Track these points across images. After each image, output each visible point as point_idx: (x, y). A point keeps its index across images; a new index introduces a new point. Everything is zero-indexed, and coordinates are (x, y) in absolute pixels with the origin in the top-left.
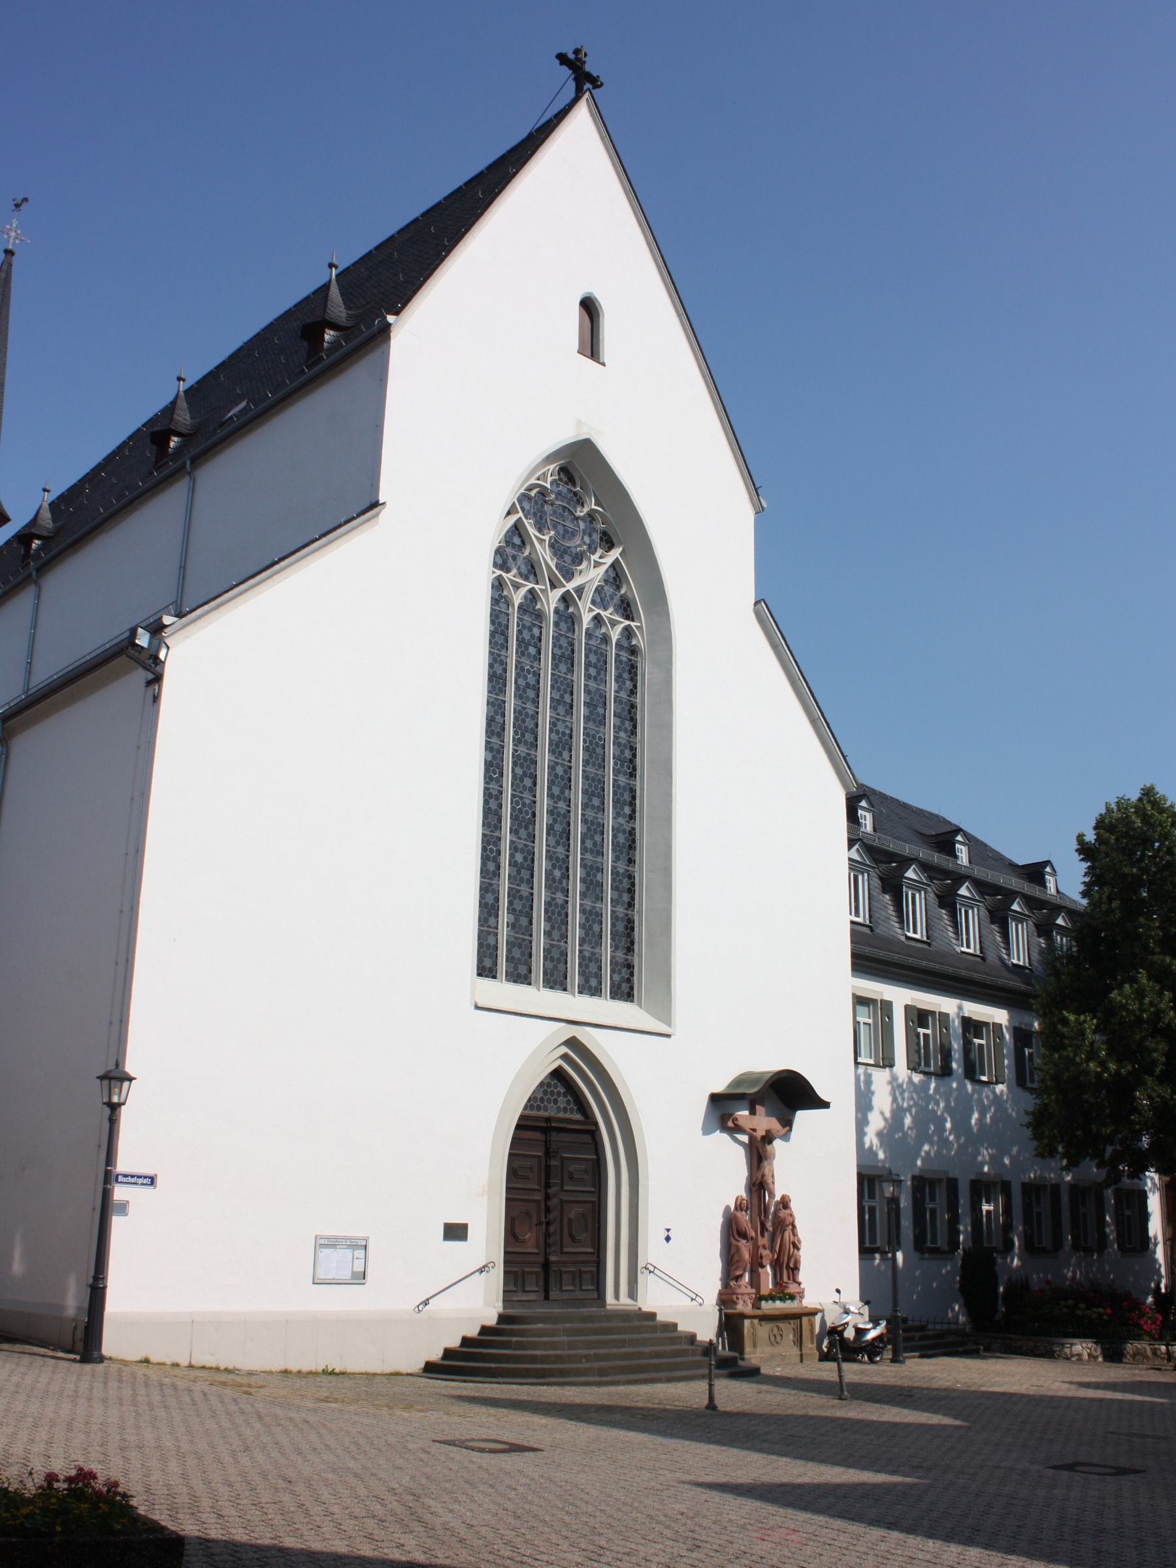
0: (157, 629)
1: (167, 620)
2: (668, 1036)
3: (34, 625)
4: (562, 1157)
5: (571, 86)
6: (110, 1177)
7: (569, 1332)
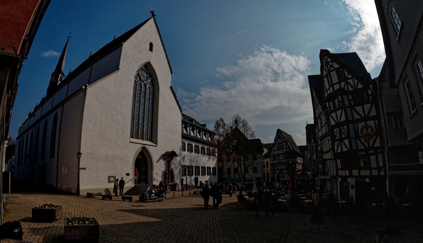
0: (86, 86)
1: (87, 85)
4: (143, 162)
5: (151, 16)
6: (79, 169)
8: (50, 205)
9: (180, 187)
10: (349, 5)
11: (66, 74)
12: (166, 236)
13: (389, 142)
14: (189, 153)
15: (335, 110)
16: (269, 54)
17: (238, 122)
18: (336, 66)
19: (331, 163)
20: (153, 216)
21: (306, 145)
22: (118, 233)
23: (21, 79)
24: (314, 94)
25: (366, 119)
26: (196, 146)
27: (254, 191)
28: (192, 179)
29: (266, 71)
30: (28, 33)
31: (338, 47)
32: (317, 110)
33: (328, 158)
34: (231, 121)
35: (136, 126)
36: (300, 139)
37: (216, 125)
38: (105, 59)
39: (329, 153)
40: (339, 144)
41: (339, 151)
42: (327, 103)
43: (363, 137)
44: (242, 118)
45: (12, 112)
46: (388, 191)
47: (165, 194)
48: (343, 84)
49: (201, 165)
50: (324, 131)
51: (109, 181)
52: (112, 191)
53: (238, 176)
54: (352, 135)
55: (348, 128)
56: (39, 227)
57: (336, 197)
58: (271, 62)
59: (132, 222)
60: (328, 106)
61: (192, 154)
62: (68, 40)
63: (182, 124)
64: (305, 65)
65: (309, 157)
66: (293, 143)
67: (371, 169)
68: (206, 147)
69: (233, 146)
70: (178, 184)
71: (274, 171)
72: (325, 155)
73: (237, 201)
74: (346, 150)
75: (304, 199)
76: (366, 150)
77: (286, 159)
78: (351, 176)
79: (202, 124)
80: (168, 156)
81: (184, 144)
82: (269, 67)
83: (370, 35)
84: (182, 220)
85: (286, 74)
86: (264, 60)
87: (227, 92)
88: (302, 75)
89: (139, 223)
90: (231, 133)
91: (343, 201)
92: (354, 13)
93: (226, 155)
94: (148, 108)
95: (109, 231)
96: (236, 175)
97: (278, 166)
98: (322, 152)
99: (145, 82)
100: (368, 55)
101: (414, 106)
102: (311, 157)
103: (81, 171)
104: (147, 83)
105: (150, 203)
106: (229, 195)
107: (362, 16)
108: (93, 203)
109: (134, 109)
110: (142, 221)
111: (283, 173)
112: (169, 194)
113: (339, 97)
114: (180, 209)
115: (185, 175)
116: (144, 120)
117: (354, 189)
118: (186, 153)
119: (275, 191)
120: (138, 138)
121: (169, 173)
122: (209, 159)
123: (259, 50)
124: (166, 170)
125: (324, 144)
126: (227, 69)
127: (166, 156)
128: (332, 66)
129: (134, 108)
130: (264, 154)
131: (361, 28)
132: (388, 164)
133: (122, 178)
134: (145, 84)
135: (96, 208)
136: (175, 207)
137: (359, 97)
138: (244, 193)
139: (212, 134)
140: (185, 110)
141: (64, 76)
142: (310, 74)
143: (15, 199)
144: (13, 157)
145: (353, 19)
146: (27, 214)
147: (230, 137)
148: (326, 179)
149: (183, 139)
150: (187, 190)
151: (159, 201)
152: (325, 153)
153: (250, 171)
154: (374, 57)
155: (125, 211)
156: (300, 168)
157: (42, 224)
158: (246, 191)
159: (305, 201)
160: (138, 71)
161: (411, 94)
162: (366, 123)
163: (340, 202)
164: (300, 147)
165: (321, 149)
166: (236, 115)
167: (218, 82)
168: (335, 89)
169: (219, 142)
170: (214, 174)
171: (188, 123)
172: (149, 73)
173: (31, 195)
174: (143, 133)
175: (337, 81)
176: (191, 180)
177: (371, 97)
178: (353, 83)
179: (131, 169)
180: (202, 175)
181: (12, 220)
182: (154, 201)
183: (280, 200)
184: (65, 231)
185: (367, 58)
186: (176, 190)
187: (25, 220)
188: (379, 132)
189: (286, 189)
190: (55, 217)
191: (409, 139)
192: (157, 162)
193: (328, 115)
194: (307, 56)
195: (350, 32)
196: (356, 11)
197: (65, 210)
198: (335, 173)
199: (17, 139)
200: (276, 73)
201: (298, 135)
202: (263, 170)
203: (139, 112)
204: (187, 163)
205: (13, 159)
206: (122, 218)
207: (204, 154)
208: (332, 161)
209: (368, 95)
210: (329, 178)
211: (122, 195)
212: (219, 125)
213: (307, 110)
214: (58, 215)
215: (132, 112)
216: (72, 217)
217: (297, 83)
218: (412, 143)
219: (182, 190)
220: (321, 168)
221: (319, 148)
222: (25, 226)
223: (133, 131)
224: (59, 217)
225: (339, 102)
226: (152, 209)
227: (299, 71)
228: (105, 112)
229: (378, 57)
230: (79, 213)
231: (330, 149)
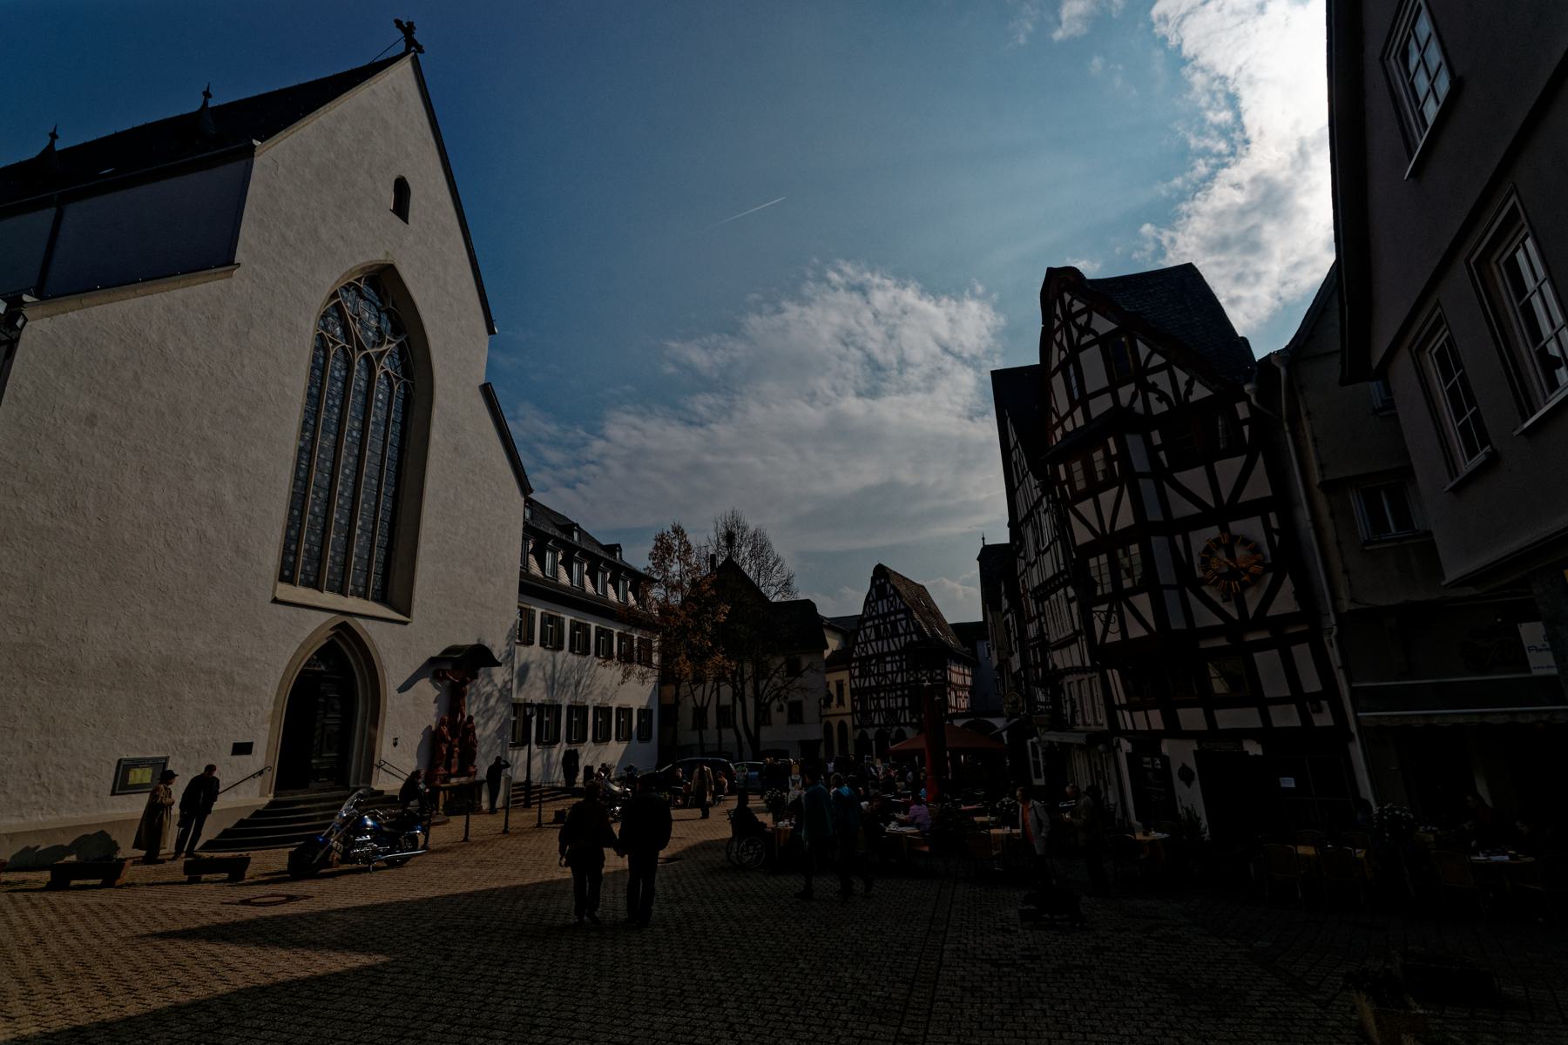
2: (405, 623)
4: (331, 693)
5: (401, 47)
7: (321, 809)
10: (1196, 56)
13: (1344, 594)
14: (548, 653)
15: (1093, 490)
16: (855, 296)
17: (738, 540)
18: (1103, 325)
19: (1085, 684)
24: (1013, 438)
25: (1223, 512)
26: (575, 626)
27: (794, 793)
28: (553, 759)
29: (842, 358)
31: (1118, 250)
32: (1019, 495)
33: (1068, 665)
34: (713, 536)
35: (311, 530)
36: (960, 599)
37: (656, 547)
39: (1074, 647)
40: (1110, 611)
41: (1114, 637)
42: (1061, 467)
43: (1216, 583)
44: (752, 524)
46: (1366, 791)
47: (426, 831)
48: (1125, 393)
50: (1049, 566)
51: (122, 786)
54: (1166, 574)
55: (1147, 553)
57: (1119, 815)
59: (222, 989)
60: (1063, 477)
61: (560, 655)
63: (525, 539)
64: (985, 331)
65: (995, 663)
66: (933, 613)
67: (1263, 705)
69: (715, 625)
71: (864, 715)
72: (1056, 655)
73: (729, 834)
74: (1142, 632)
75: (984, 825)
76: (1232, 629)
77: (907, 671)
78: (1173, 730)
79: (604, 543)
81: (526, 615)
82: (853, 343)
83: (1266, 181)
85: (911, 370)
86: (835, 318)
87: (701, 431)
88: (970, 371)
91: (1154, 835)
92: (1213, 94)
93: (689, 657)
94: (377, 460)
96: (724, 731)
97: (879, 699)
98: (1044, 645)
99: (370, 351)
100: (1246, 264)
101: (1475, 434)
102: (1004, 664)
104: (380, 355)
106: (698, 812)
107: (1247, 100)
110: (281, 978)
111: (898, 724)
113: (1111, 441)
115: (524, 741)
117: (1196, 784)
119: (872, 791)
121: (454, 736)
122: (626, 675)
123: (822, 279)
124: (442, 723)
126: (705, 348)
127: (448, 667)
128: (1085, 329)
129: (306, 452)
130: (827, 653)
131: (1232, 154)
132: (1349, 681)
134: (367, 357)
137: (1191, 433)
138: (755, 802)
139: (640, 582)
140: (546, 490)
142: (1000, 364)
145: (1203, 120)
148: (1071, 745)
151: (392, 864)
152: (1054, 649)
153: (779, 717)
154: (1275, 268)
155: (189, 934)
156: (964, 704)
158: (762, 794)
159: (993, 831)
160: (334, 295)
161: (1462, 397)
162: (1224, 529)
163: (1139, 836)
164: (958, 628)
165: (1041, 633)
166: (729, 514)
167: (668, 395)
169: (665, 609)
170: (645, 734)
171: (550, 537)
172: (388, 312)
174: (346, 564)
175: (1105, 383)
176: (547, 765)
177: (1246, 429)
178: (1172, 383)
180: (595, 740)
182: (366, 865)
183: (892, 827)
185: (1239, 279)
188: (1287, 557)
189: (915, 786)
191: (1451, 576)
192: (403, 688)
193: (1063, 509)
194: (995, 296)
195: (1178, 182)
196: (1223, 79)
198: (1103, 720)
200: (874, 367)
201: (949, 583)
202: (824, 712)
204: (536, 693)
207: (609, 657)
208: (1086, 677)
209: (1235, 423)
210: (1081, 739)
211: (190, 853)
212: (669, 549)
213: (983, 496)
217: (951, 402)
218: (1470, 591)
220: (1044, 704)
221: (1032, 630)
223: (296, 554)
225: (1108, 459)
226: (346, 910)
227: (958, 356)
229: (1296, 266)
231: (1077, 633)
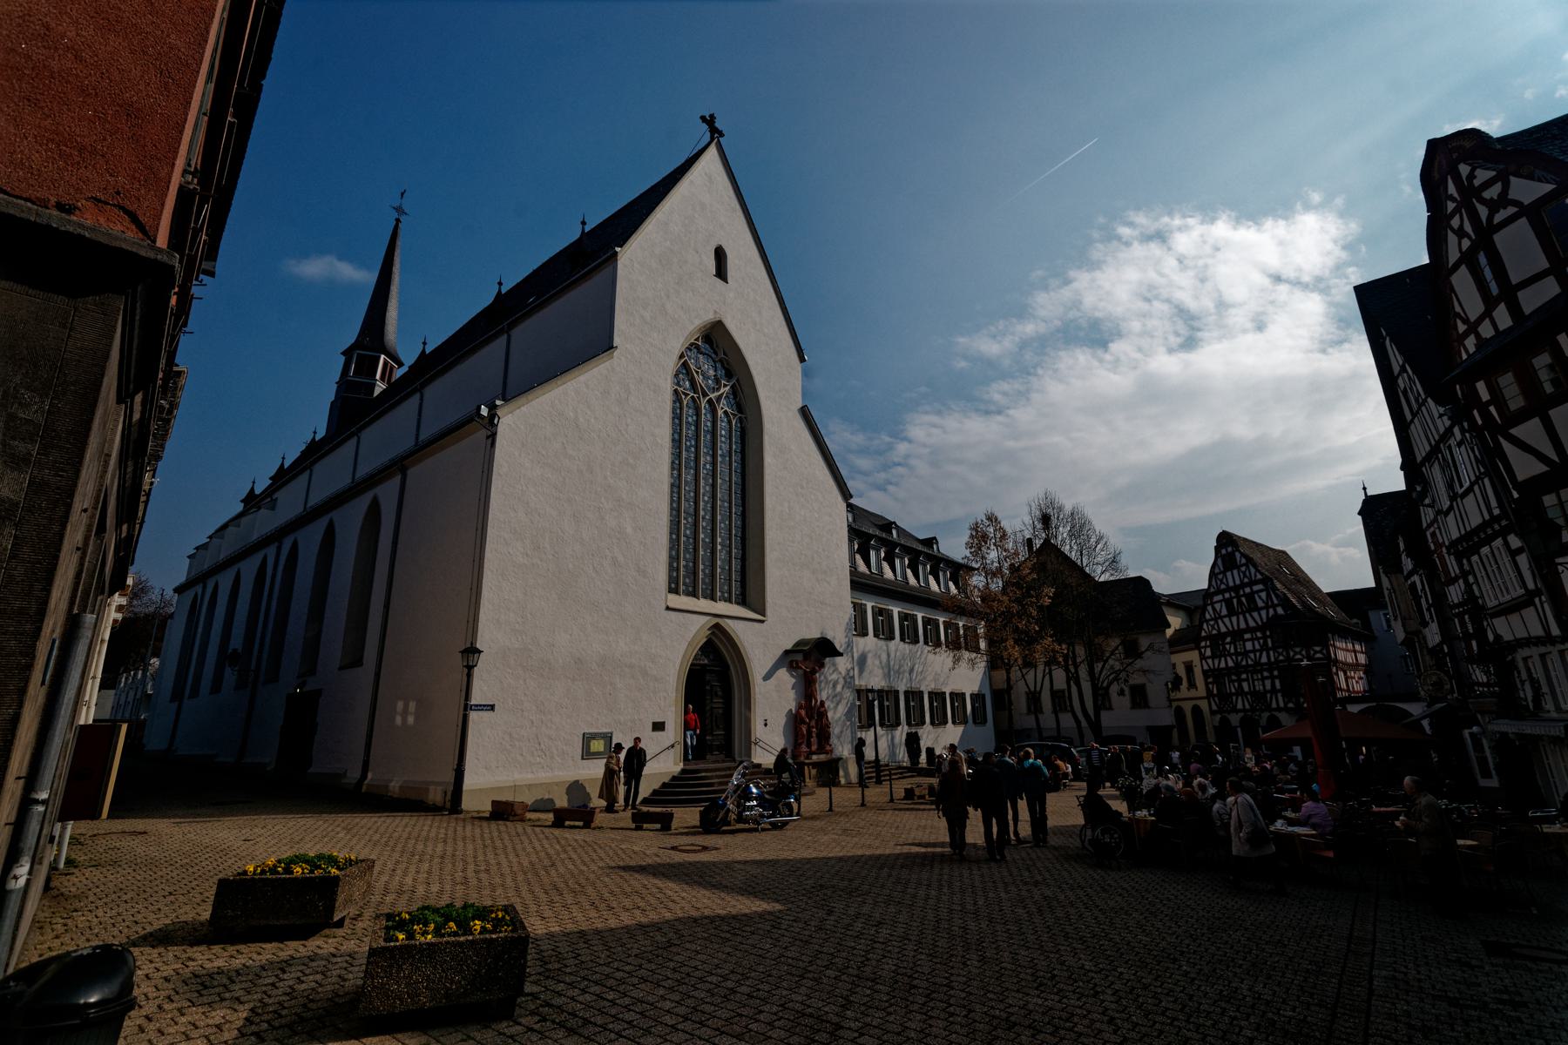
0: (493, 408)
1: (498, 402)
3: (505, 383)
4: (714, 681)
8: (320, 857)
9: (853, 770)
11: (409, 357)
12: (802, 977)
14: (882, 643)
17: (1054, 522)
20: (749, 890)
21: (1371, 584)
22: (607, 970)
23: (189, 353)
24: (1396, 359)
26: (904, 617)
28: (897, 740)
29: (1144, 315)
30: (196, 161)
32: (1416, 430)
34: (1028, 520)
35: (686, 549)
36: (1340, 561)
37: (972, 536)
38: (556, 305)
45: (159, 482)
47: (798, 800)
49: (926, 687)
51: (587, 754)
52: (594, 791)
53: (1072, 723)
56: (237, 963)
58: (1162, 275)
59: (668, 915)
62: (398, 221)
63: (851, 541)
66: (1300, 580)
68: (941, 620)
69: (1041, 608)
70: (846, 761)
71: (1224, 700)
77: (1274, 648)
80: (807, 656)
81: (859, 609)
82: (1157, 297)
84: (865, 909)
85: (1233, 311)
86: (1132, 275)
87: (1000, 418)
89: (695, 920)
90: (1029, 564)
94: (726, 486)
95: (571, 962)
97: (1240, 681)
102: (1414, 638)
103: (473, 715)
104: (719, 398)
105: (740, 837)
108: (516, 840)
109: (679, 493)
110: (707, 912)
112: (814, 800)
114: (857, 860)
115: (870, 723)
116: (713, 530)
118: (869, 642)
120: (694, 594)
122: (957, 661)
124: (800, 707)
125: (1480, 574)
127: (799, 657)
128: (1504, 200)
129: (676, 487)
130: (1169, 632)
133: (637, 740)
134: (710, 402)
135: (526, 863)
136: (837, 852)
139: (958, 571)
140: (861, 496)
141: (400, 364)
143: (126, 843)
144: (155, 662)
146: (188, 908)
147: (1029, 579)
148: (1540, 737)
149: (858, 594)
150: (879, 782)
151: (775, 826)
155: (641, 869)
156: (1359, 686)
157: (255, 947)
160: (682, 356)
164: (1338, 597)
166: (1042, 495)
168: (1527, 310)
169: (987, 596)
172: (721, 361)
173: (228, 821)
174: (713, 575)
176: (892, 746)
179: (669, 704)
180: (932, 723)
181: (81, 945)
184: (368, 974)
186: (838, 784)
187: (161, 939)
190: (331, 909)
192: (767, 677)
197: (384, 878)
199: (179, 590)
201: (1318, 548)
202: (1173, 695)
203: (696, 503)
204: (876, 681)
205: (151, 670)
206: (627, 903)
207: (938, 644)
211: (634, 807)
212: (985, 537)
214: (349, 901)
215: (672, 501)
216: (414, 908)
219: (862, 783)
220: (1487, 685)
221: (1455, 593)
222: (153, 970)
223: (678, 569)
224: (353, 911)
228: (568, 505)
230: (448, 887)
